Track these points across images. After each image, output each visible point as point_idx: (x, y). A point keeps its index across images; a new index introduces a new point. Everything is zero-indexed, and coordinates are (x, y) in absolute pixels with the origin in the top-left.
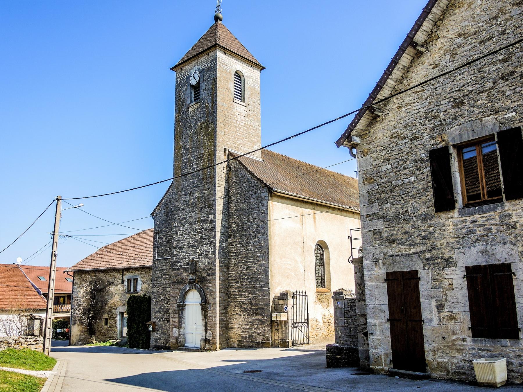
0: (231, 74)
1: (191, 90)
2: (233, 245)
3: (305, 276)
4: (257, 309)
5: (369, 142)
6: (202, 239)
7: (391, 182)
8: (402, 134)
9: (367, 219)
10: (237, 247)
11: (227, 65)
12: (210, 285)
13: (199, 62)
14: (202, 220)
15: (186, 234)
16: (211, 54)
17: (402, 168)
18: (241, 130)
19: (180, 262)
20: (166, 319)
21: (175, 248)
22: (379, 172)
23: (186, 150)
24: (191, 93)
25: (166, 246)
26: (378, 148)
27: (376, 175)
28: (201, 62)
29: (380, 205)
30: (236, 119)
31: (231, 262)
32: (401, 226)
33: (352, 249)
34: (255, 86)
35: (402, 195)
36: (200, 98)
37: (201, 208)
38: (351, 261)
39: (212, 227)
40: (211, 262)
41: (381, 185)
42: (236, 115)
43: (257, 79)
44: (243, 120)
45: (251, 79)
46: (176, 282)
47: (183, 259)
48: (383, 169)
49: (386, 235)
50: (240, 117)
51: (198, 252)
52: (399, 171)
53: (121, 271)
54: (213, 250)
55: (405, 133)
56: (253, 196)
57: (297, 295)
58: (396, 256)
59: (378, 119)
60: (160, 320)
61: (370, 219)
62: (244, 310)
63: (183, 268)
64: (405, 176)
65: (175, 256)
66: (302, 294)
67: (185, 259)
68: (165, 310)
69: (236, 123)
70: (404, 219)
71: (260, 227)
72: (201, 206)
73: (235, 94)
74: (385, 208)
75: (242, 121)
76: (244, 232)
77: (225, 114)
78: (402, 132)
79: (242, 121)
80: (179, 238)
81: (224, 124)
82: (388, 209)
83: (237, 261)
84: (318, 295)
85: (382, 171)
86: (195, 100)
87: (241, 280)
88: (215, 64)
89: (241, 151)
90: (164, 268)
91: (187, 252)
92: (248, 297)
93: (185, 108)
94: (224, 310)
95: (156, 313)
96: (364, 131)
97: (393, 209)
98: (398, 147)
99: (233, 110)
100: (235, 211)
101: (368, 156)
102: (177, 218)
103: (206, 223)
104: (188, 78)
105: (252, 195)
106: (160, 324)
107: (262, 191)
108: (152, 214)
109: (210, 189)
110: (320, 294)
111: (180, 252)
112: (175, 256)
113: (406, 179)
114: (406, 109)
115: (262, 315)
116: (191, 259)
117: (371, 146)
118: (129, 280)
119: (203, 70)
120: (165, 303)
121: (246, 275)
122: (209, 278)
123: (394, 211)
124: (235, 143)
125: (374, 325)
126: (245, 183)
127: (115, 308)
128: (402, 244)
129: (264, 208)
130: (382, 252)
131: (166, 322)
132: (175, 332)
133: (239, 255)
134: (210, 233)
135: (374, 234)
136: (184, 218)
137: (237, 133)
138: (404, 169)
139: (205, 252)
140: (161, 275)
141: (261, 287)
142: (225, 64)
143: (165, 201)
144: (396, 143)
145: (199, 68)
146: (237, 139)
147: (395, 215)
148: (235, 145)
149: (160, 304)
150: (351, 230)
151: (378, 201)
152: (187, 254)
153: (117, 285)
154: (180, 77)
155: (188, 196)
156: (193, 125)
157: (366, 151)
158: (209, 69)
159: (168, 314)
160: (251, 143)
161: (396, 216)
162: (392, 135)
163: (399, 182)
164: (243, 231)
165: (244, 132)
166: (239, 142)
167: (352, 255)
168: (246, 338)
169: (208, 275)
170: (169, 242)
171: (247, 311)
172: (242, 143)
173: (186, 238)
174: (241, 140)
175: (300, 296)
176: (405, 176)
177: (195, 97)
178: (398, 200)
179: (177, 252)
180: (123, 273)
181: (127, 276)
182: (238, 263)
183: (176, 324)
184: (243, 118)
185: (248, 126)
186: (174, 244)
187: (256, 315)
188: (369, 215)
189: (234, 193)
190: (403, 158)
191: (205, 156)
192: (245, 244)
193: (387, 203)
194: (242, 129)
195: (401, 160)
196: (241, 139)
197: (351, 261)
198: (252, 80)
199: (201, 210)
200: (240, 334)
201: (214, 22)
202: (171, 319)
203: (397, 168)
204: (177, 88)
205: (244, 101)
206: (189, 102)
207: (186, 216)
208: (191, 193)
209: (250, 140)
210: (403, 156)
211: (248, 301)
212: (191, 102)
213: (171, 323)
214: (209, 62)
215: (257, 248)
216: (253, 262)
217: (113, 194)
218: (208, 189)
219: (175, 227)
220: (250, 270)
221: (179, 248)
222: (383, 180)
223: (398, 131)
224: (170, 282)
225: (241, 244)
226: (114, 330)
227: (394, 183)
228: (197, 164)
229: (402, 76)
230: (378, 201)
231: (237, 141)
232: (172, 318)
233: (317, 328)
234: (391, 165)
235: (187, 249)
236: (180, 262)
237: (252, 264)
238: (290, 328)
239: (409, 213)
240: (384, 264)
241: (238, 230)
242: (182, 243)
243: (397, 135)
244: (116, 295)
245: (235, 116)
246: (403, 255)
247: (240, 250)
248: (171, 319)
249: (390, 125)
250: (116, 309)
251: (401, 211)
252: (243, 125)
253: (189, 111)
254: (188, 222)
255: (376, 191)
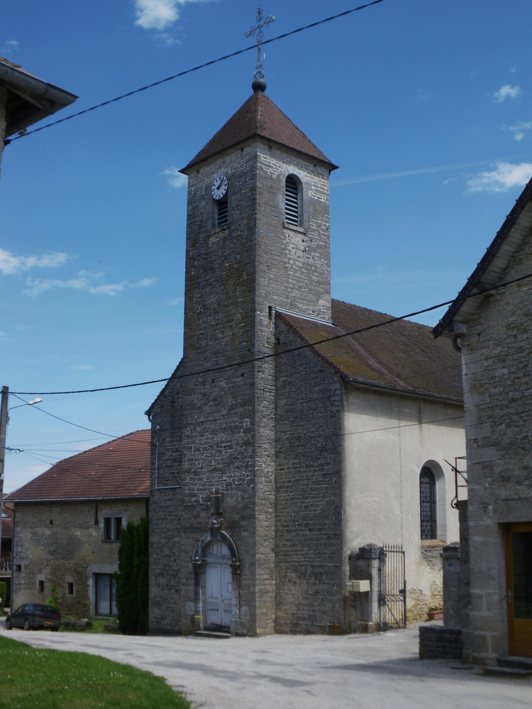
0: (280, 181)
1: (213, 207)
2: (283, 470)
3: (402, 520)
4: (322, 574)
5: (478, 332)
6: (232, 459)
7: (507, 393)
8: (522, 325)
9: (475, 445)
10: (289, 472)
11: (274, 166)
12: (245, 534)
13: (227, 162)
14: (231, 427)
15: (205, 449)
16: (247, 150)
17: (521, 375)
18: (297, 275)
19: (195, 495)
20: (174, 586)
21: (188, 471)
22: (492, 378)
23: (205, 307)
24: (213, 212)
25: (172, 466)
26: (491, 342)
27: (487, 381)
28: (229, 161)
29: (492, 427)
30: (289, 256)
31: (281, 497)
32: (518, 457)
33: (457, 486)
34: (321, 199)
35: (521, 413)
36: (229, 221)
37: (231, 406)
38: (455, 504)
39: (248, 440)
40: (246, 496)
41: (494, 397)
42: (288, 250)
43: (323, 185)
44: (299, 257)
45: (313, 187)
46: (189, 528)
47: (200, 490)
48: (498, 373)
49: (499, 469)
50: (296, 253)
51: (225, 480)
52: (518, 378)
53: (94, 505)
54: (250, 478)
55: (526, 323)
56: (317, 389)
57: (386, 551)
58: (512, 500)
59: (492, 299)
60: (163, 588)
61: (478, 446)
62: (302, 575)
63: (201, 505)
64: (525, 387)
65: (187, 484)
66: (395, 550)
67: (205, 490)
68: (171, 572)
69: (288, 263)
70: (523, 449)
71: (327, 441)
72: (230, 404)
73: (287, 214)
74: (498, 431)
75: (299, 259)
76: (301, 448)
77: (270, 248)
78: (522, 321)
79: (299, 259)
80: (194, 455)
81: (268, 266)
82: (502, 432)
83: (289, 496)
84: (424, 552)
85: (496, 377)
86: (219, 223)
87: (297, 528)
88: (253, 166)
89: (297, 310)
90: (170, 503)
91: (207, 479)
92: (307, 554)
93: (202, 236)
94: (268, 574)
95: (156, 577)
96: (472, 315)
97: (509, 432)
98: (517, 344)
99: (284, 241)
100: (287, 412)
101: (478, 353)
102: (190, 422)
103: (239, 432)
104: (209, 188)
105: (314, 386)
106: (163, 594)
107: (330, 380)
108: (148, 413)
109: (245, 376)
110: (428, 549)
111: (195, 479)
112: (187, 484)
113: (526, 390)
114: (528, 288)
115: (330, 584)
116: (214, 490)
117: (482, 339)
118: (108, 521)
119: (234, 174)
120: (171, 561)
121: (304, 519)
122: (243, 523)
123: (510, 436)
124: (287, 297)
125: (480, 597)
126: (304, 366)
127: (85, 565)
128: (519, 483)
129: (334, 409)
130: (492, 494)
131: (173, 591)
132: (190, 607)
133: (293, 486)
134: (245, 450)
135: (484, 468)
136: (202, 422)
137: (290, 280)
138: (525, 376)
139: (238, 480)
140: (165, 515)
141: (329, 538)
142: (269, 166)
143: (169, 392)
144: (515, 336)
145: (227, 172)
146: (289, 290)
147: (512, 441)
148: (286, 300)
149: (164, 563)
150: (456, 458)
151: (490, 420)
152: (207, 482)
153: (87, 528)
154: (195, 184)
155: (207, 386)
156: (217, 266)
157: (475, 344)
158: (243, 174)
159: (177, 580)
160: (314, 294)
161: (512, 444)
162: (510, 325)
163: (517, 395)
164: (299, 446)
165: (302, 276)
166: (293, 295)
167: (457, 496)
168: (304, 619)
169: (243, 518)
170: (179, 460)
171: (305, 576)
172: (299, 296)
173: (205, 456)
174: (297, 292)
175: (392, 553)
176: (525, 387)
177: (219, 219)
178: (516, 420)
179: (191, 478)
180: (97, 508)
181: (104, 513)
182: (292, 499)
183: (192, 595)
184: (301, 254)
185: (309, 267)
186: (186, 465)
187: (320, 583)
188: (477, 441)
189: (284, 381)
190: (523, 360)
191: (237, 320)
192: (303, 467)
193: (501, 424)
194: (299, 272)
195: (520, 362)
196: (297, 290)
197: (455, 504)
198: (315, 188)
199: (230, 410)
200: (295, 612)
201: (251, 92)
202: (183, 588)
203: (515, 373)
204: (190, 203)
205: (301, 225)
206: (209, 227)
207: (205, 419)
208: (213, 381)
209: (313, 290)
210: (523, 357)
211: (308, 561)
212: (214, 226)
213: (183, 593)
214: (243, 162)
215: (323, 475)
216: (316, 498)
217: (94, 391)
218: (242, 375)
219: (188, 436)
220: (310, 511)
221: (194, 472)
222: (497, 390)
223: (516, 320)
224: (179, 527)
225: (296, 468)
226: (84, 603)
227: (511, 395)
228: (223, 332)
229: (523, 240)
230: (490, 420)
231: (290, 294)
232: (185, 585)
233: (421, 604)
234: (508, 368)
235: (207, 474)
236: (195, 495)
237: (315, 501)
238: (375, 605)
239: (529, 439)
240: (495, 511)
241: (291, 445)
242: (199, 464)
243: (516, 325)
244: (86, 545)
245: (287, 252)
246: (520, 499)
247: (294, 477)
248: (183, 588)
249: (507, 310)
250: (86, 568)
251: (519, 437)
252: (299, 265)
253: (210, 242)
254: (209, 429)
255: (487, 405)
